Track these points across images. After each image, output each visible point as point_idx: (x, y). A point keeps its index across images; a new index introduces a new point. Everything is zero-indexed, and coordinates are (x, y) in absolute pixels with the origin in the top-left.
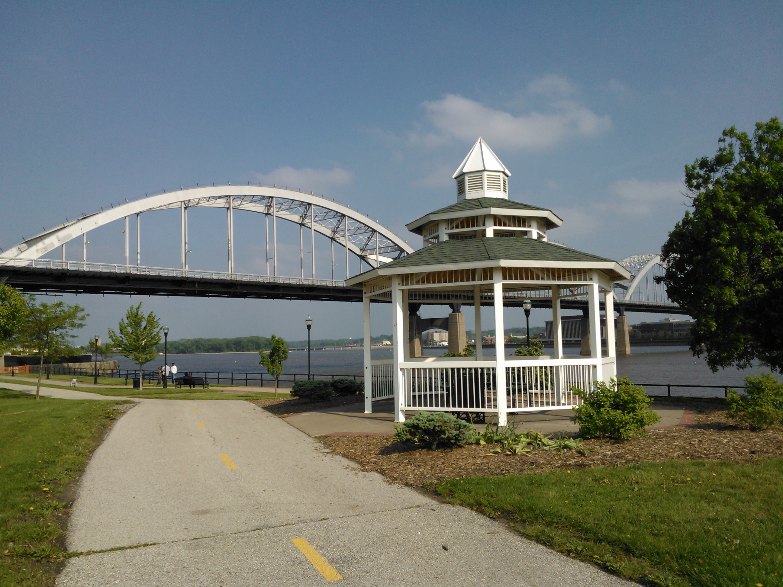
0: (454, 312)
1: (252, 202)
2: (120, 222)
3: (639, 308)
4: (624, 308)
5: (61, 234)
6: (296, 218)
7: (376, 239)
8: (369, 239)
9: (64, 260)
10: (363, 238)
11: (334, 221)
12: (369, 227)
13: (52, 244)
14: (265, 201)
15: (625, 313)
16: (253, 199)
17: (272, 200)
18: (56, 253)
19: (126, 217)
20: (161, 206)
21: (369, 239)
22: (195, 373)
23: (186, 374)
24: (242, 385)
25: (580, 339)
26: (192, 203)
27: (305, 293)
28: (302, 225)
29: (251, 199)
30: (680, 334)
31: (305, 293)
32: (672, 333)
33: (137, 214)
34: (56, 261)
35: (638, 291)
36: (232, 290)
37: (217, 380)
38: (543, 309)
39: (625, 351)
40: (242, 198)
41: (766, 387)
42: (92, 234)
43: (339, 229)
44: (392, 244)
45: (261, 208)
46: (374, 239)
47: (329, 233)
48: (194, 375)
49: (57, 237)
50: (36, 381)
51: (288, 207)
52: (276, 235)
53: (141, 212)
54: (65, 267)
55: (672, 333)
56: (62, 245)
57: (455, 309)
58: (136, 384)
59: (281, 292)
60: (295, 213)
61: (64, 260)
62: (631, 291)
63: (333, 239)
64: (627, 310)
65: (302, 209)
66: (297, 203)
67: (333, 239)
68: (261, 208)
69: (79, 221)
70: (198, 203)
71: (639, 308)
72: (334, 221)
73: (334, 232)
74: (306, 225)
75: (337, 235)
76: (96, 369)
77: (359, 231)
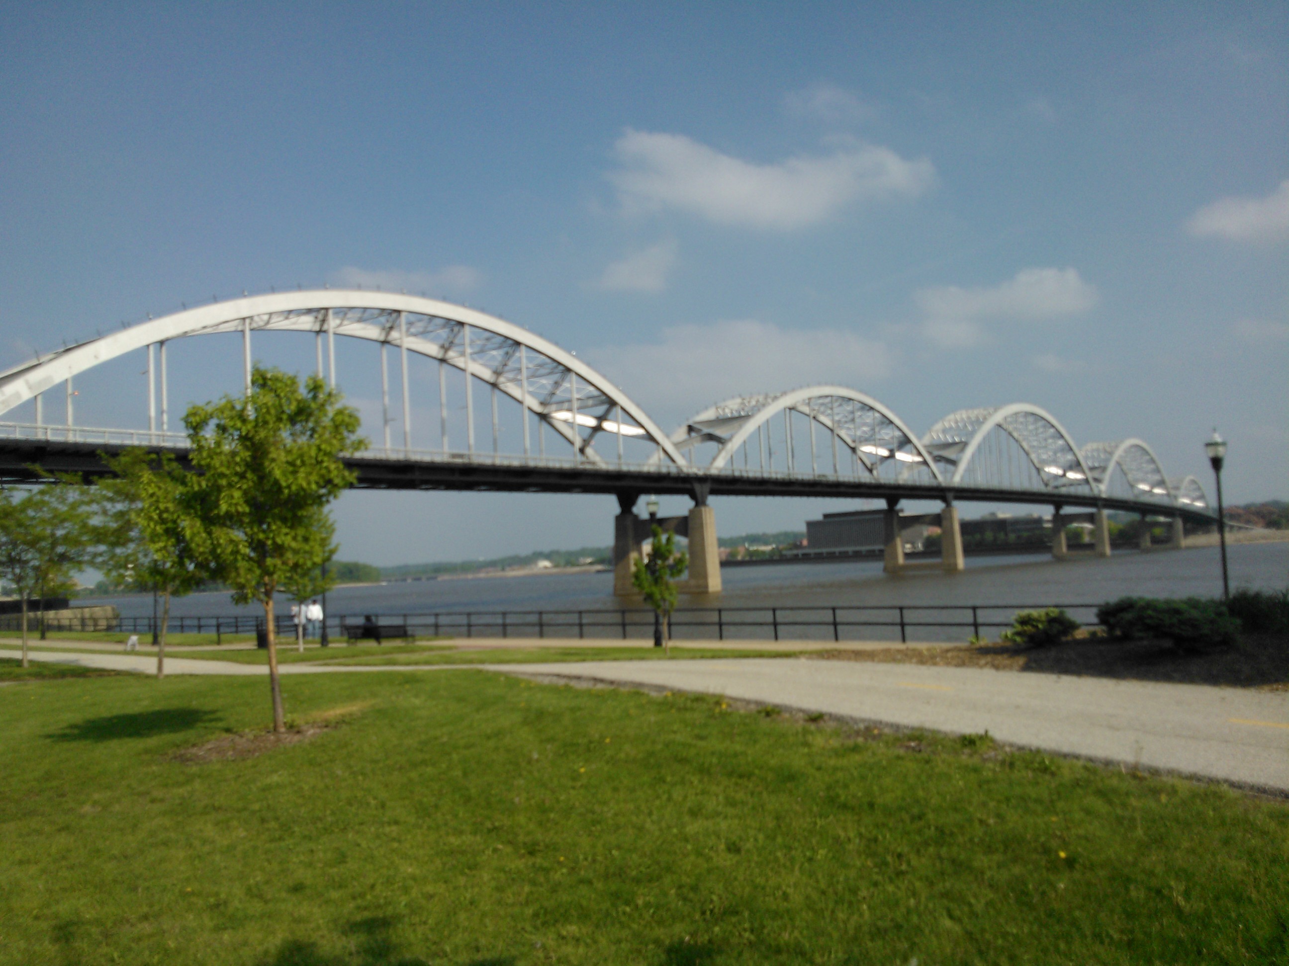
0: (697, 504)
1: (360, 320)
2: (137, 357)
3: (988, 495)
4: (707, 487)
5: (34, 376)
6: (433, 349)
7: (571, 385)
8: (557, 384)
9: (40, 423)
10: (546, 382)
11: (498, 354)
12: (559, 364)
13: (18, 395)
14: (383, 319)
15: (712, 500)
16: (365, 314)
17: (326, 315)
18: (26, 409)
19: (148, 346)
20: (205, 327)
21: (557, 384)
22: (126, 620)
23: (368, 618)
24: (459, 635)
25: (881, 547)
26: (256, 322)
27: (457, 478)
28: (443, 361)
29: (359, 315)
30: (1019, 537)
31: (807, 489)
32: (1006, 535)
33: (162, 343)
34: (28, 425)
35: (970, 470)
36: (408, 477)
37: (899, 628)
38: (751, 499)
39: (956, 565)
40: (343, 312)
41: (70, 619)
42: (82, 379)
43: (507, 368)
44: (596, 393)
45: (373, 332)
46: (566, 385)
47: (487, 374)
48: (383, 622)
49: (27, 382)
50: (19, 642)
51: (421, 330)
52: (168, 367)
53: (167, 340)
54: (41, 436)
55: (1006, 535)
56: (36, 397)
57: (699, 502)
58: (262, 641)
59: (417, 476)
60: (433, 340)
61: (40, 423)
62: (962, 466)
63: (494, 385)
64: (714, 492)
65: (444, 333)
66: (454, 323)
67: (494, 385)
68: (373, 332)
69: (59, 355)
70: (268, 323)
71: (988, 495)
72: (498, 354)
73: (497, 373)
74: (450, 361)
75: (502, 379)
76: (155, 618)
77: (542, 371)
